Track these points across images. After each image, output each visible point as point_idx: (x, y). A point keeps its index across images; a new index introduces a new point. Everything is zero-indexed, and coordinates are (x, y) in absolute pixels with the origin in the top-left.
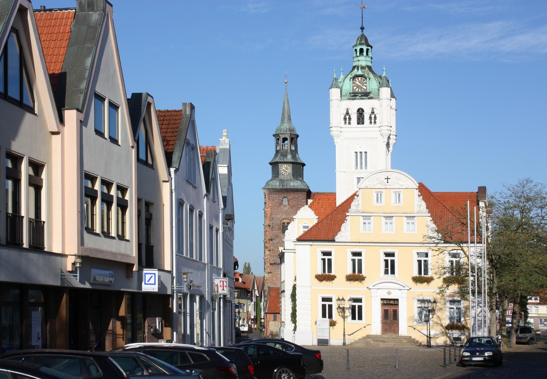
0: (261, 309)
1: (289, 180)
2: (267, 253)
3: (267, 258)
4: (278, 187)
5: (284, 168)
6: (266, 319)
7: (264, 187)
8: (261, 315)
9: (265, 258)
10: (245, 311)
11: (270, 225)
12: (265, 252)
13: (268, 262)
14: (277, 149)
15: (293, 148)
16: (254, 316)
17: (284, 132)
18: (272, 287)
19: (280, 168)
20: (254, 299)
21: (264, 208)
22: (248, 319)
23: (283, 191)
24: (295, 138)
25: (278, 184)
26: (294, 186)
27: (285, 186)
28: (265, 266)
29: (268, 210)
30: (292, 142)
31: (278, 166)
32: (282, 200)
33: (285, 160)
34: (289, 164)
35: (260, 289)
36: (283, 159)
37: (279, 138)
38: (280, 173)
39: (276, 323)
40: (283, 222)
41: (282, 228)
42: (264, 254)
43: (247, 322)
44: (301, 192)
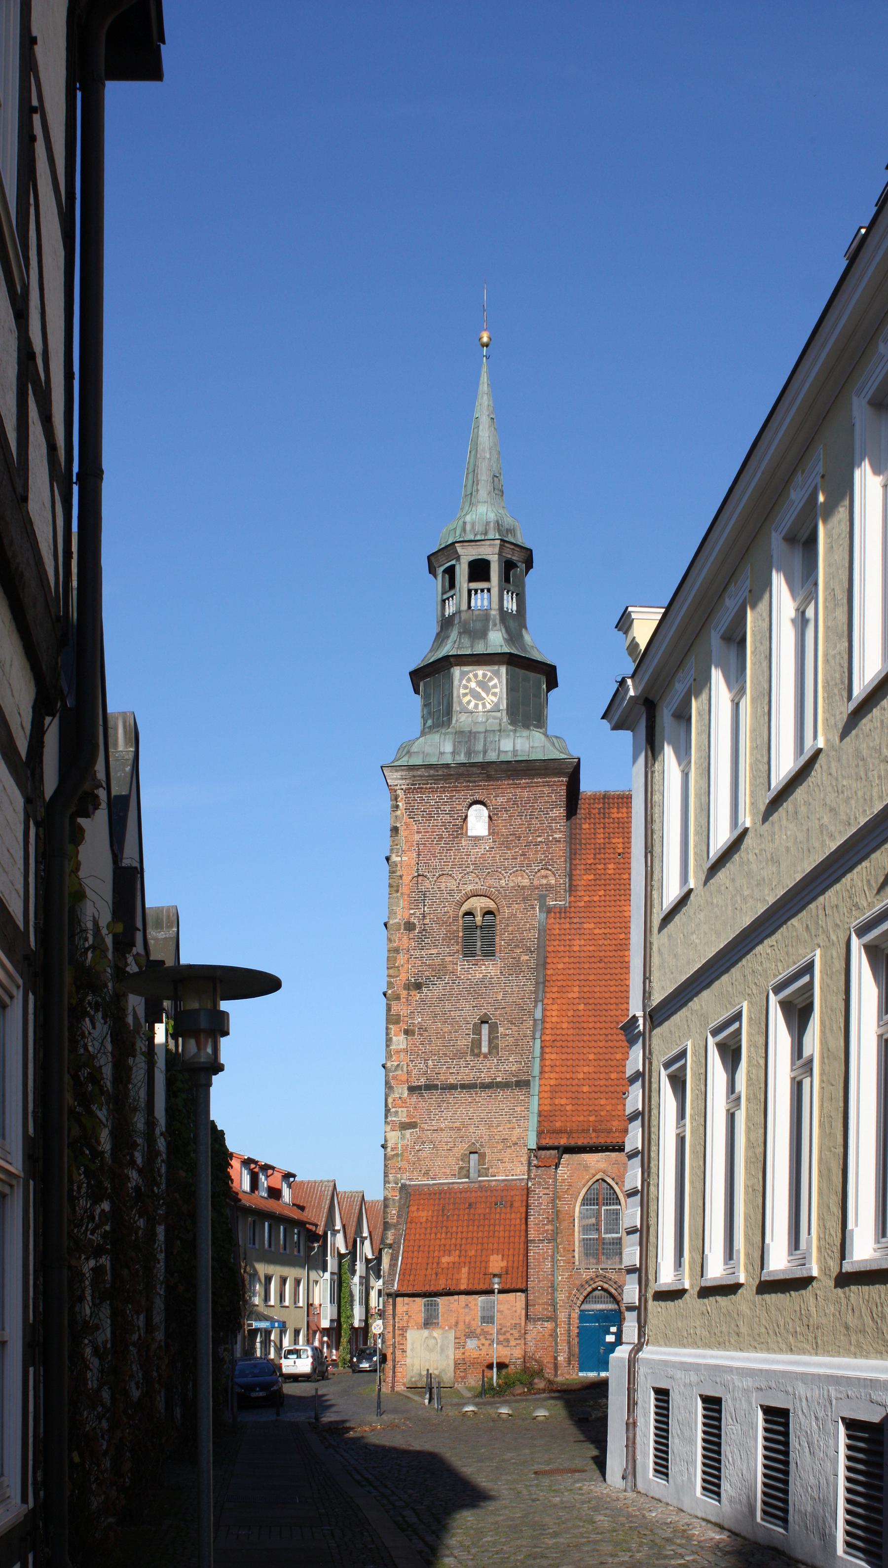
0: (352, 1295)
1: (494, 731)
2: (400, 1041)
3: (396, 1064)
4: (448, 759)
5: (473, 685)
6: (394, 1318)
7: (393, 762)
8: (352, 1316)
9: (389, 1065)
10: (301, 1304)
11: (414, 924)
12: (389, 1041)
13: (403, 1082)
14: (443, 615)
15: (510, 605)
16: (332, 1321)
17: (475, 535)
18: (415, 1185)
19: (456, 682)
20: (332, 1263)
21: (388, 854)
22: (311, 1332)
23: (469, 775)
24: (519, 564)
25: (448, 747)
26: (515, 751)
27: (478, 752)
28: (390, 1100)
29: (405, 858)
30: (507, 580)
31: (450, 678)
32: (466, 816)
33: (480, 649)
34: (496, 667)
35: (351, 1232)
36: (472, 647)
37: (453, 562)
38: (456, 707)
39: (435, 1334)
40: (465, 908)
41: (461, 934)
42: (388, 1046)
43: (308, 1340)
44: (545, 775)
